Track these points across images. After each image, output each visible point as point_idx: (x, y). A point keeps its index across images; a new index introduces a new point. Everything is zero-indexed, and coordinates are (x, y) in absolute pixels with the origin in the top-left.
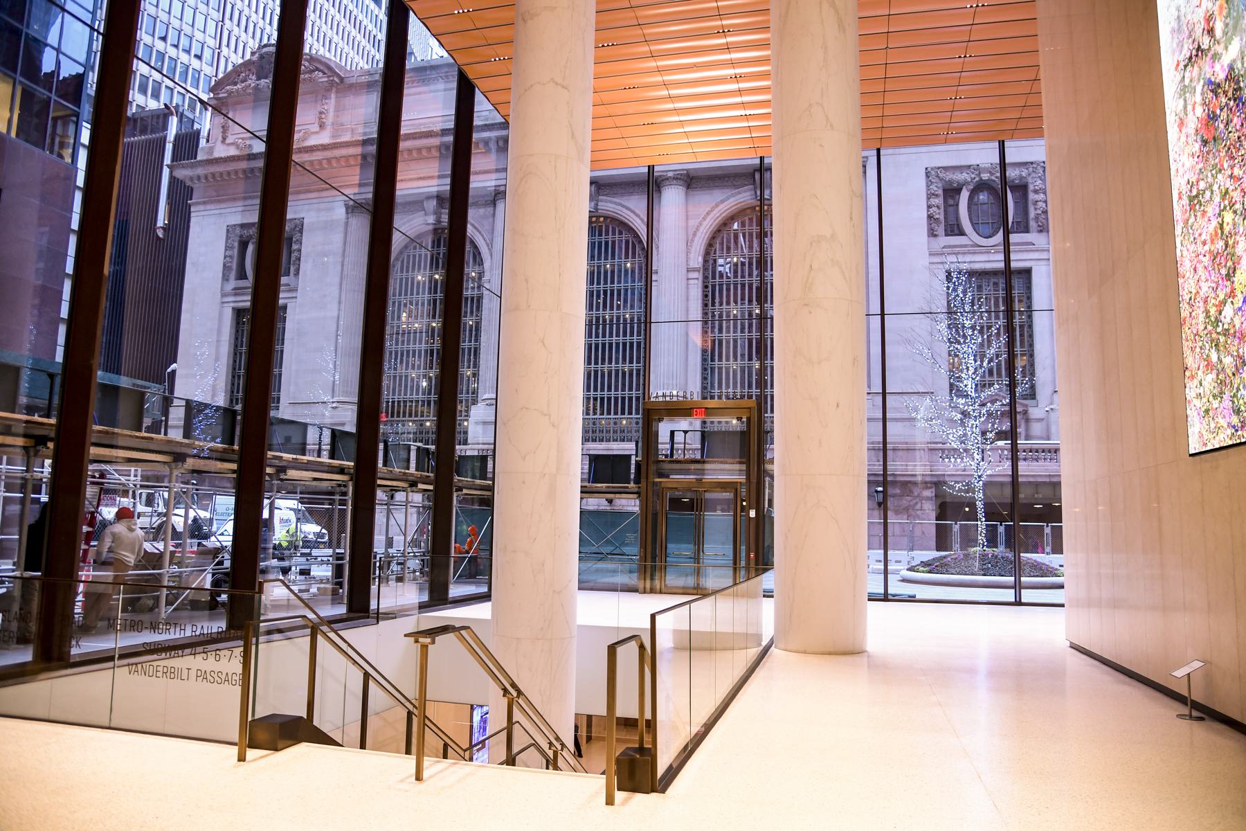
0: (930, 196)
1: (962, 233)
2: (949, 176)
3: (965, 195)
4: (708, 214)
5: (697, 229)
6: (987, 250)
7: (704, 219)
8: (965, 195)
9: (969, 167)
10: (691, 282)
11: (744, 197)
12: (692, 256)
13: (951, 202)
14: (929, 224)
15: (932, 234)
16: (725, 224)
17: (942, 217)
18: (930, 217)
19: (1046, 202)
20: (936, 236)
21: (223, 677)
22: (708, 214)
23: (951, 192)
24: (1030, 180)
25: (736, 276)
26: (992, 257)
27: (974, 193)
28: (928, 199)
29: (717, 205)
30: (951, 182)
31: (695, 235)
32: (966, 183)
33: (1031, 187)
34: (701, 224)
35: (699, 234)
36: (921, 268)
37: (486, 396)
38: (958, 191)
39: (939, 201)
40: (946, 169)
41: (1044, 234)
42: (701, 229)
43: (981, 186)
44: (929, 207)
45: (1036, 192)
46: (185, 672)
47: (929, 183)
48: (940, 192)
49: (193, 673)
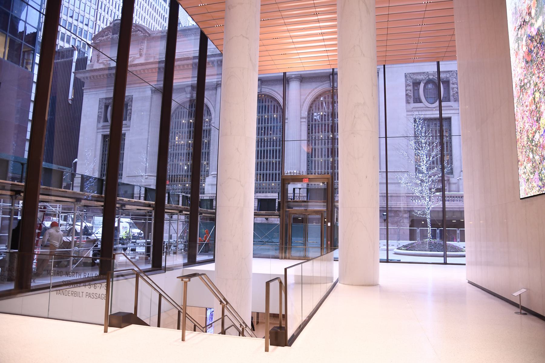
0: (407, 85)
1: (421, 102)
2: (415, 77)
3: (422, 85)
4: (310, 93)
5: (305, 100)
6: (432, 109)
7: (308, 95)
8: (422, 85)
9: (424, 73)
10: (302, 123)
11: (325, 86)
12: (303, 112)
13: (416, 88)
14: (407, 98)
15: (408, 102)
16: (317, 98)
17: (412, 95)
18: (407, 95)
19: (457, 88)
20: (409, 103)
21: (98, 296)
22: (310, 93)
23: (416, 84)
24: (450, 79)
25: (322, 121)
26: (434, 112)
27: (426, 84)
28: (406, 87)
29: (314, 90)
30: (416, 80)
31: (304, 103)
32: (422, 80)
33: (451, 82)
34: (306, 98)
35: (306, 102)
36: (403, 117)
37: (212, 173)
38: (419, 83)
39: (411, 88)
40: (414, 74)
41: (457, 102)
42: (307, 100)
43: (429, 81)
44: (406, 90)
45: (453, 84)
46: (81, 294)
47: (406, 80)
48: (411, 84)
49: (84, 294)
